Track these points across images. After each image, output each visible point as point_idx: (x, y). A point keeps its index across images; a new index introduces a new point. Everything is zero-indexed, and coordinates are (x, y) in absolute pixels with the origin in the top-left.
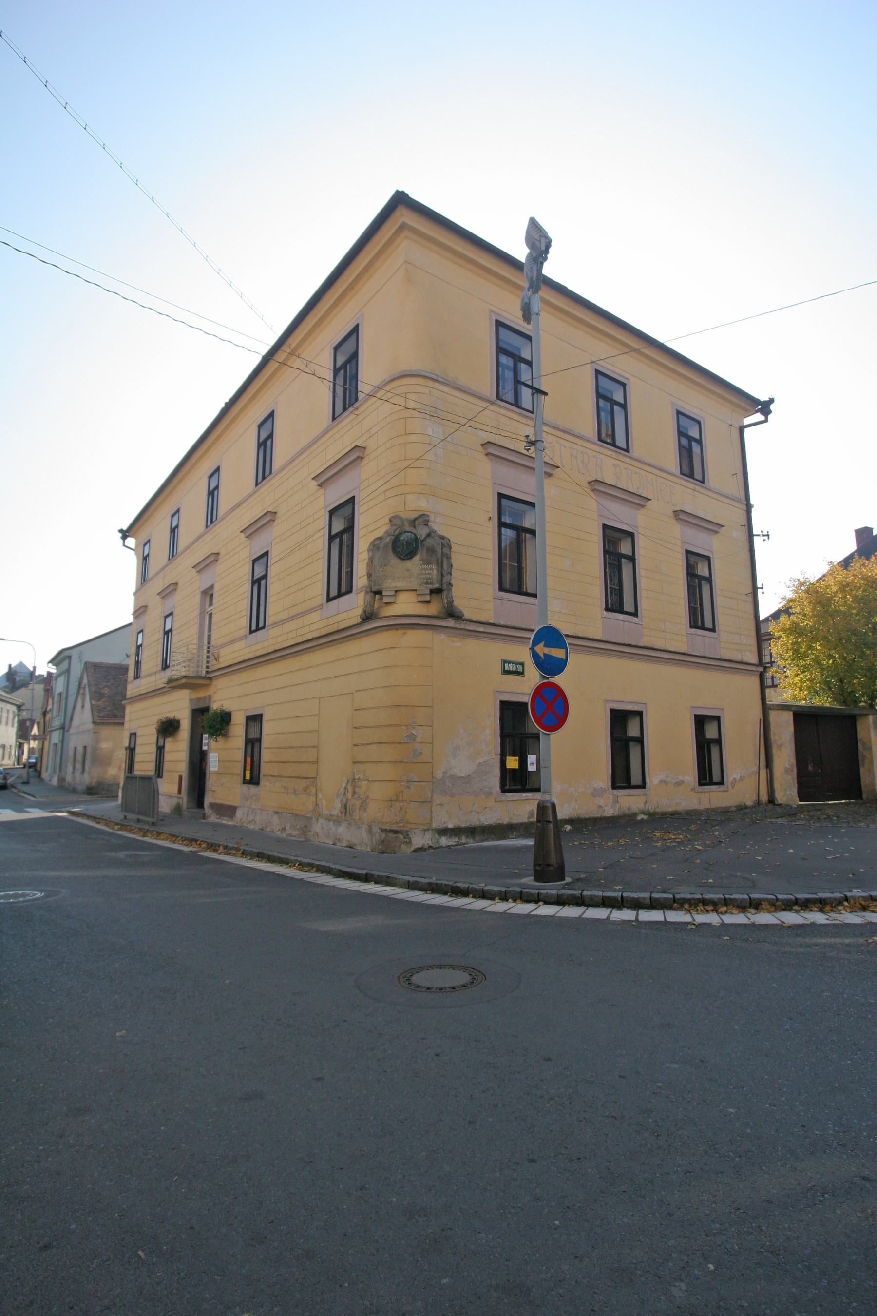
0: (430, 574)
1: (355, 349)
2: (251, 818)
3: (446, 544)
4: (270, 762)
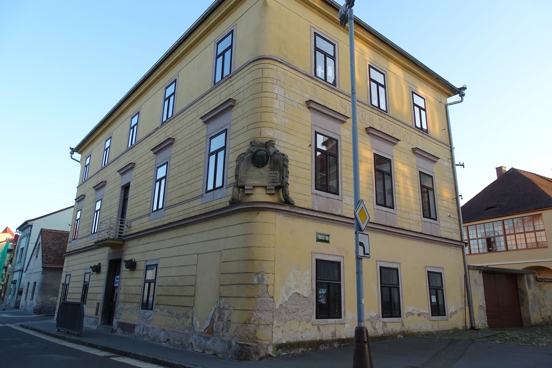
0: (275, 177)
1: (230, 44)
2: (145, 333)
3: (284, 158)
4: (161, 295)
